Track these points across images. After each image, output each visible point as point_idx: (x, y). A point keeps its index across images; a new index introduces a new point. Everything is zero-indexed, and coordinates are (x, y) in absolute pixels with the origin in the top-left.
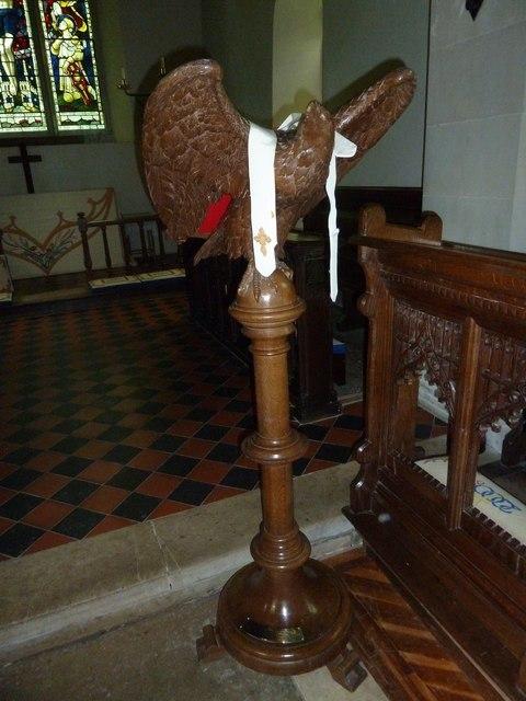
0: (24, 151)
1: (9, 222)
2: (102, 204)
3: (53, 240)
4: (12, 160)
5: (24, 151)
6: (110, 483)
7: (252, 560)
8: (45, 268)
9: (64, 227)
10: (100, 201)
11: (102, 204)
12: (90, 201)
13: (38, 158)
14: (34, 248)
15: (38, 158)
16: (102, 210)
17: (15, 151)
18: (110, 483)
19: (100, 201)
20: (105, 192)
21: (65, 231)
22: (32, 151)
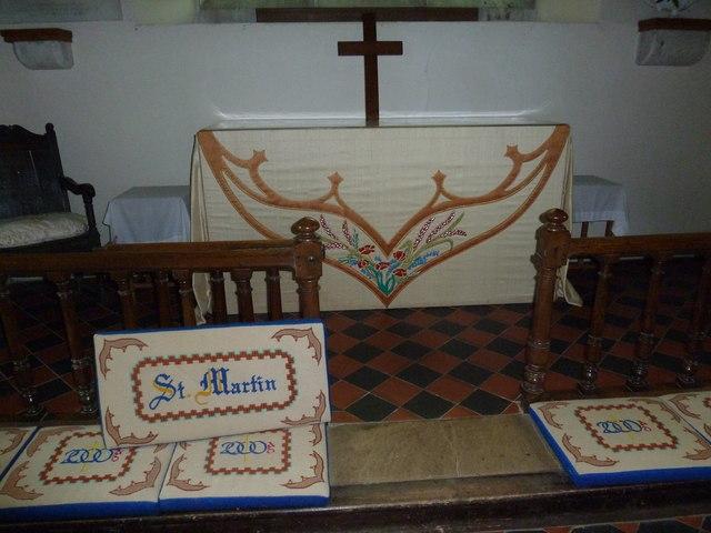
0: (370, 32)
1: (328, 185)
2: (384, 283)
3: (412, 235)
4: (345, 49)
5: (370, 32)
6: (439, 375)
7: (362, 57)
8: (385, 294)
9: (443, 208)
10: (533, 156)
11: (384, 283)
12: (512, 153)
13: (395, 48)
14: (367, 250)
15: (395, 48)
16: (534, 174)
17: (354, 32)
18: (439, 375)
19: (533, 156)
20: (550, 131)
21: (440, 217)
22: (386, 32)
